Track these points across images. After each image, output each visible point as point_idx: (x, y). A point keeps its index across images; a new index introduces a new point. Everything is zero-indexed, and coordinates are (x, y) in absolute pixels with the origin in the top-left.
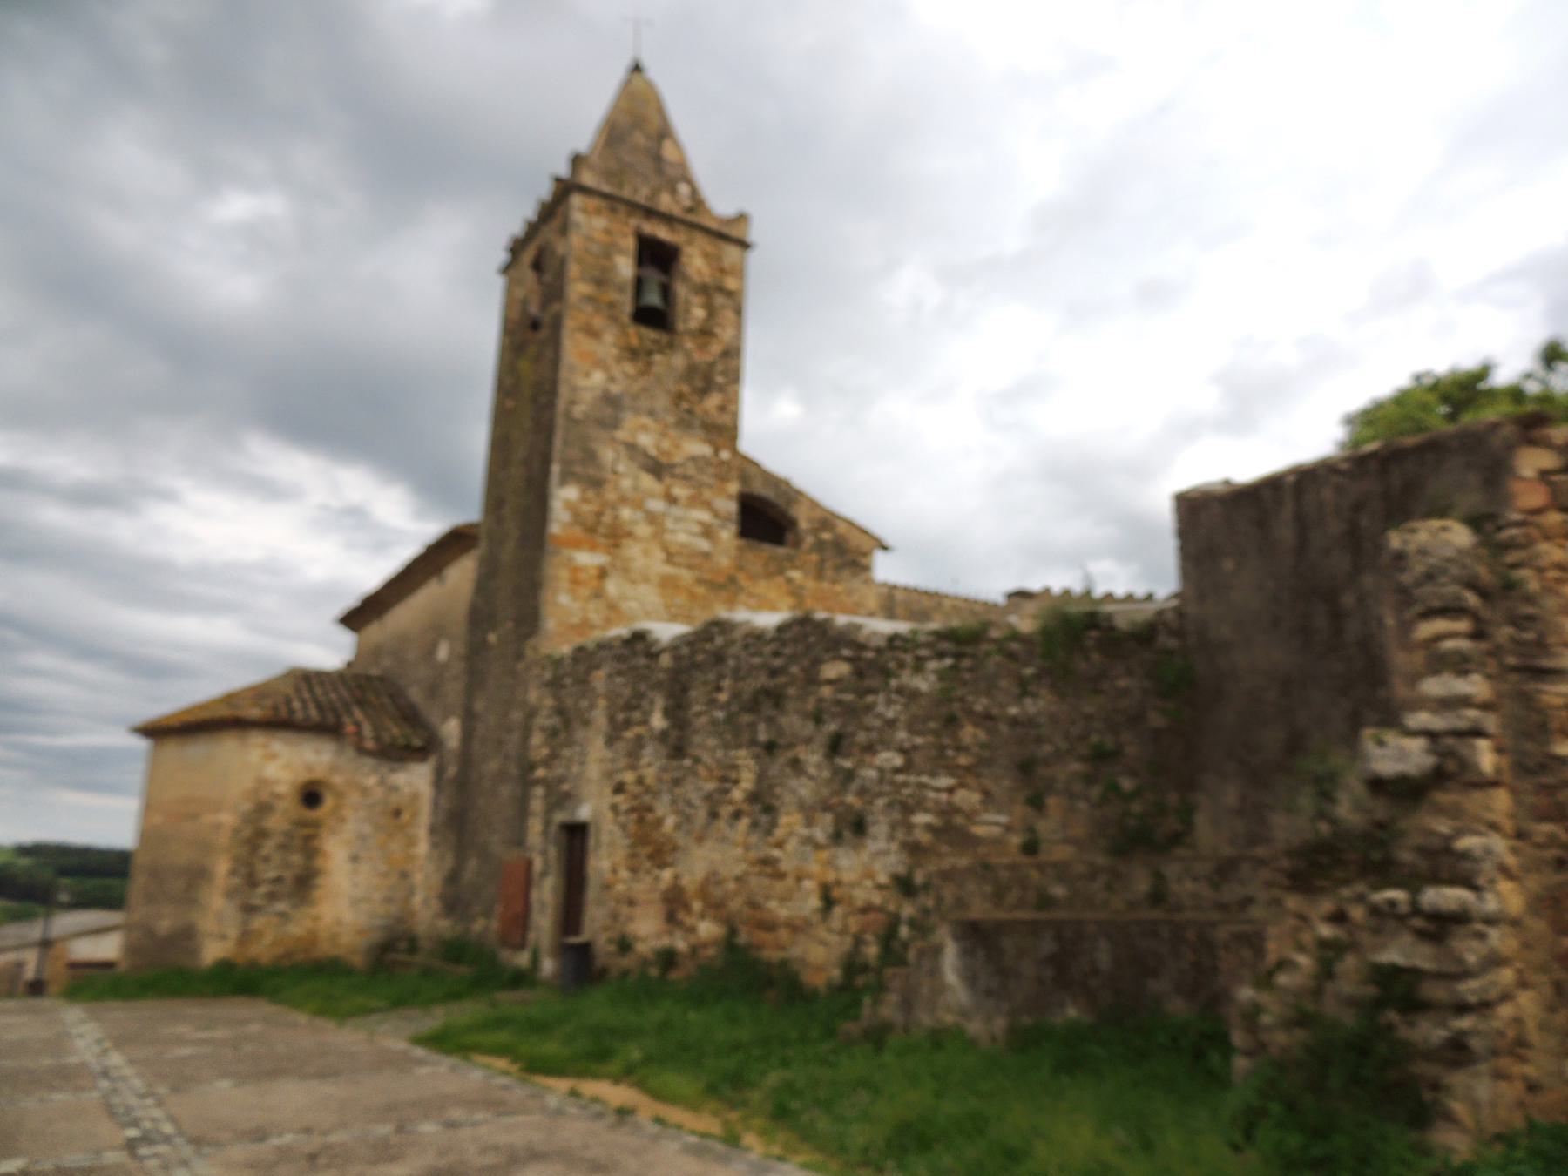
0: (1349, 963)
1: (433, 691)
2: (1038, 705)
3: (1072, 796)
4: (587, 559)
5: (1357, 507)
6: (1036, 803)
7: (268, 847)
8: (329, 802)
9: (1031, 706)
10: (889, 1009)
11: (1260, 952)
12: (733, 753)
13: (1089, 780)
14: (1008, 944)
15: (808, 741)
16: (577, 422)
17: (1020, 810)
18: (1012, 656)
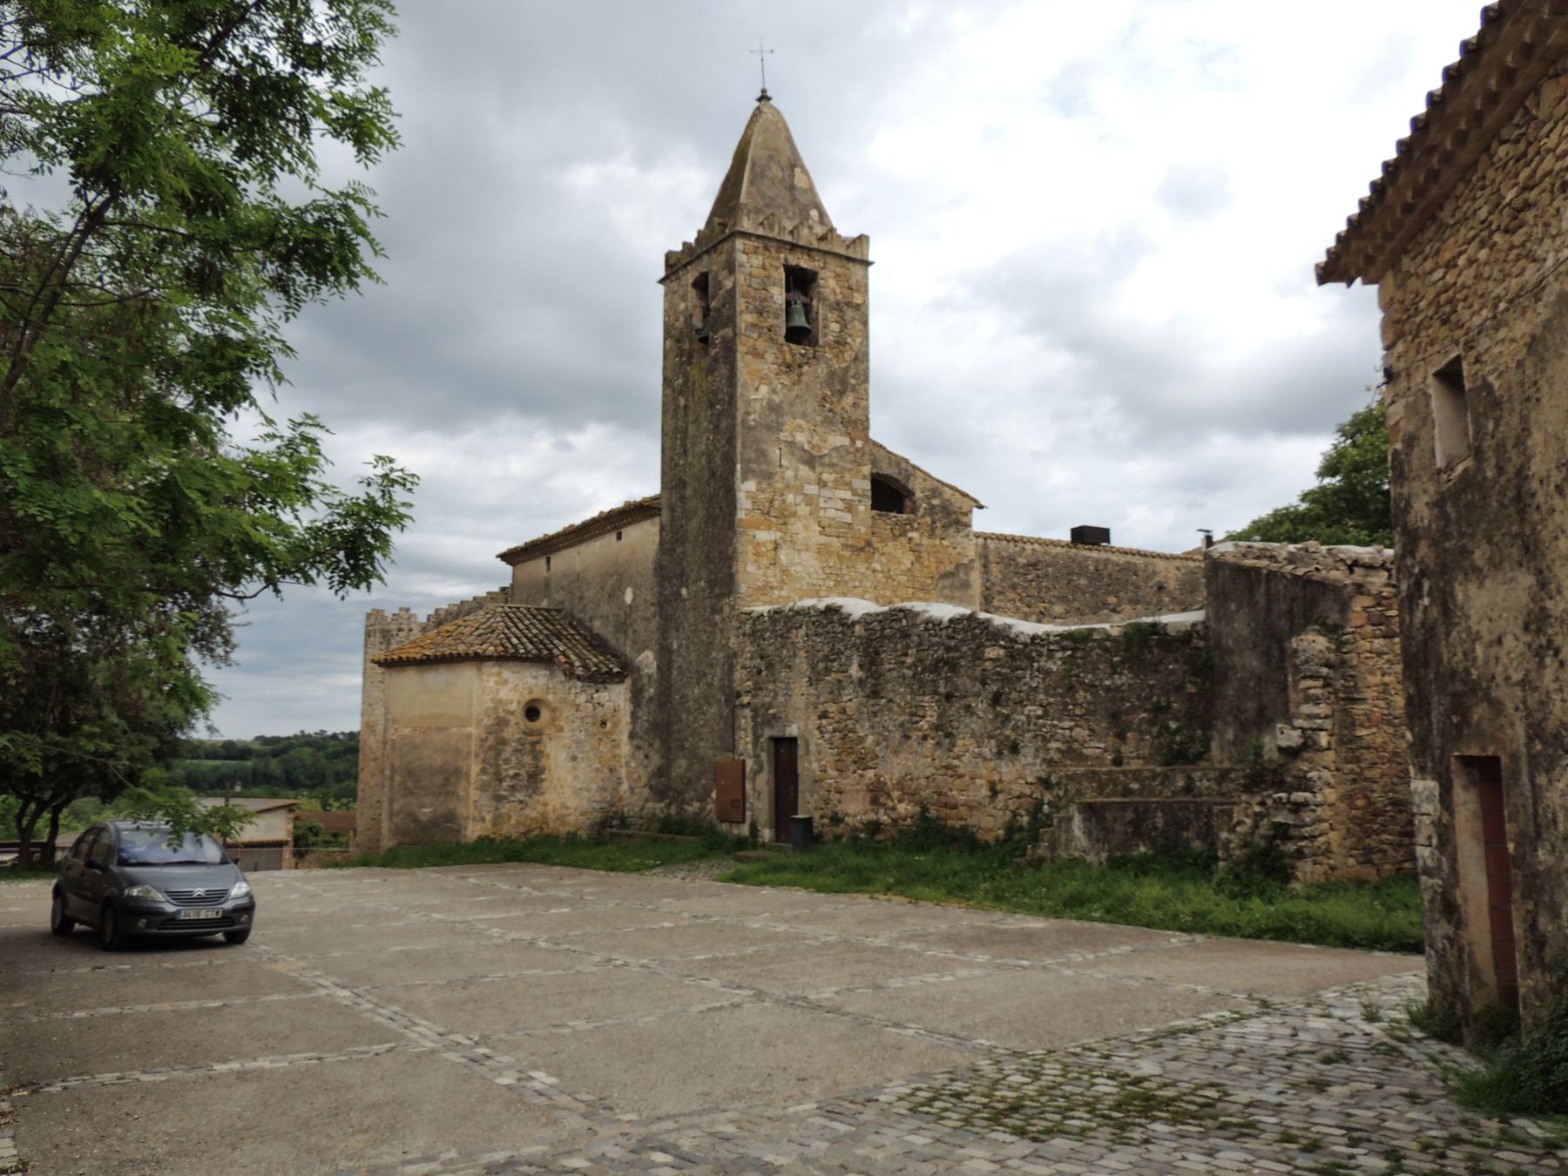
0: (1265, 821)
1: (622, 627)
2: (1123, 679)
3: (1141, 732)
4: (764, 536)
5: (1293, 600)
6: (1121, 736)
7: (507, 752)
8: (545, 715)
9: (1118, 680)
10: (1042, 850)
11: (1231, 818)
12: (919, 698)
13: (1152, 723)
14: (1108, 815)
15: (978, 695)
16: (752, 428)
17: (1111, 740)
18: (1106, 650)
